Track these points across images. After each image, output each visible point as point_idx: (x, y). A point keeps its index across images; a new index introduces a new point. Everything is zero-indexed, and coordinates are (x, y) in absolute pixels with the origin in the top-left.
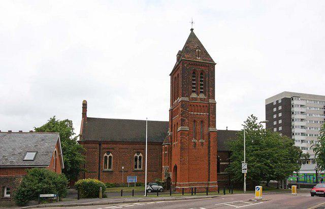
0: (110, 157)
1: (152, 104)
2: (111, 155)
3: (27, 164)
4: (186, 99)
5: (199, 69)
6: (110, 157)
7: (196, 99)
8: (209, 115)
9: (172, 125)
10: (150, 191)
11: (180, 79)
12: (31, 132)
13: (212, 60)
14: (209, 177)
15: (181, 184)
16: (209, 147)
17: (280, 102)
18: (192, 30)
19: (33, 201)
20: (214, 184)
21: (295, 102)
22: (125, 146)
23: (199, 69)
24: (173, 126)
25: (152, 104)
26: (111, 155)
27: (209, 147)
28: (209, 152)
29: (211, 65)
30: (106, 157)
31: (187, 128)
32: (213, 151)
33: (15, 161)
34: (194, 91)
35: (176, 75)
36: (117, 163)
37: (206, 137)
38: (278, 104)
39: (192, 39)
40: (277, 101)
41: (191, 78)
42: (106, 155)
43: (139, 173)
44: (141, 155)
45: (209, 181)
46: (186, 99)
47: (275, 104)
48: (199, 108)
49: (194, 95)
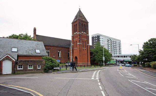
0: (49, 52)
1: (66, 34)
2: (60, 51)
3: (37, 54)
4: (80, 33)
5: (84, 23)
6: (49, 52)
7: (83, 34)
8: (87, 40)
9: (73, 41)
10: (68, 66)
11: (78, 26)
12: (8, 37)
13: (87, 21)
14: (88, 61)
15: (79, 63)
16: (88, 51)
17: (96, 36)
18: (80, 9)
19: (51, 71)
20: (89, 64)
21: (101, 37)
22: (54, 48)
23: (84, 23)
24: (74, 42)
25: (66, 34)
26: (49, 51)
27: (88, 51)
28: (88, 52)
29: (87, 23)
30: (59, 52)
31: (81, 43)
32: (89, 52)
33: (31, 53)
34: (82, 31)
35: (75, 24)
36: (52, 54)
37: (86, 47)
38: (96, 37)
39: (80, 12)
40: (95, 36)
41: (82, 26)
42: (58, 52)
43: (60, 59)
44: (49, 51)
45: (88, 62)
46: (80, 33)
47: (95, 37)
48: (82, 37)
49: (82, 32)
